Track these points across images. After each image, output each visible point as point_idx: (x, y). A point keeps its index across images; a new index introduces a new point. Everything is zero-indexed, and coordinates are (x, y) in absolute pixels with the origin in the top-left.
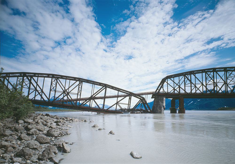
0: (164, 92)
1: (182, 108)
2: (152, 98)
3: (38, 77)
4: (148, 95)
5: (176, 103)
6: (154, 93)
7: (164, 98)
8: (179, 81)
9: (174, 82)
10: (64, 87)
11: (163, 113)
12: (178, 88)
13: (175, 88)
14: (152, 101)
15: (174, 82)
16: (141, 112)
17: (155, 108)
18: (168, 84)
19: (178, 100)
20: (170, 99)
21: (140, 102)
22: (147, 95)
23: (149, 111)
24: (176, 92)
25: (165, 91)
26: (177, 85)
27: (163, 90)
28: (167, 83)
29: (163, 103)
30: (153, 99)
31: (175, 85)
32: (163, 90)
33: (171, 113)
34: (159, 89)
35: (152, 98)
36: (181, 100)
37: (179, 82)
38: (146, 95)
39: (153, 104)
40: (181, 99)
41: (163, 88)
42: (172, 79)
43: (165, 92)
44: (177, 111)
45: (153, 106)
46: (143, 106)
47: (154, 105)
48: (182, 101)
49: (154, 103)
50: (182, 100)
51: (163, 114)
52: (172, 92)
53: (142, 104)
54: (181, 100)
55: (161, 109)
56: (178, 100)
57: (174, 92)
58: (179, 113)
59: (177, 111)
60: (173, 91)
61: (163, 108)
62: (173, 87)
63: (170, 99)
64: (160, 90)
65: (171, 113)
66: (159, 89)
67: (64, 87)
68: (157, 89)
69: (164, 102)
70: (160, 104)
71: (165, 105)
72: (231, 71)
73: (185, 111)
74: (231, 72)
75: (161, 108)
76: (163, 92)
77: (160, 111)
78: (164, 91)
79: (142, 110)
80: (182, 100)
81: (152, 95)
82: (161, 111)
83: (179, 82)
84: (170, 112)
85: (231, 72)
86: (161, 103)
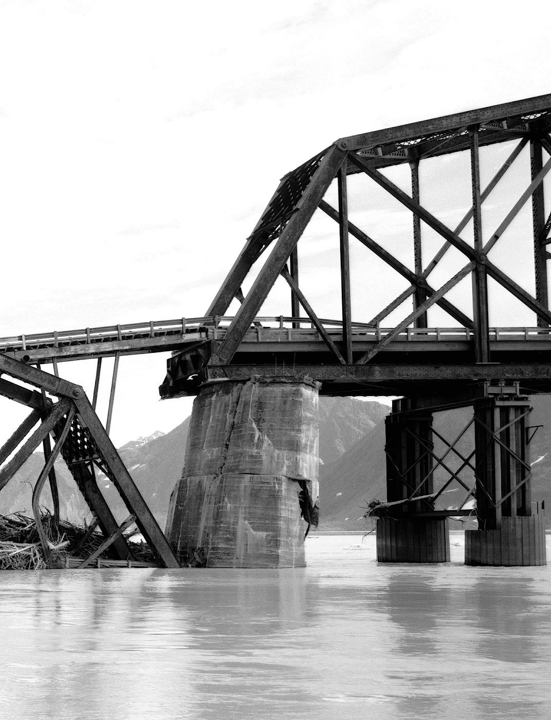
0: (306, 326)
1: (514, 506)
2: (168, 390)
3: (415, 157)
4: (123, 359)
5: (439, 449)
6: (188, 337)
7: (307, 392)
8: (478, 198)
9: (420, 215)
10: (483, 189)
11: (289, 562)
12: (469, 279)
13: (435, 281)
14: (167, 432)
15: (420, 215)
16: (45, 553)
17: (207, 510)
18: (347, 229)
19: (466, 414)
20: (368, 403)
21: (33, 444)
22: (108, 362)
23: (138, 539)
24: (438, 318)
25: (320, 314)
26: (452, 238)
27: (297, 298)
28: (340, 216)
29: (294, 446)
30: (184, 405)
31: (432, 241)
32: (297, 298)
33: (383, 559)
34: (247, 286)
35: (168, 390)
36: (497, 412)
37: (475, 213)
38: (99, 355)
39: (181, 464)
40: (498, 403)
41: (293, 278)
42: (399, 174)
43: (312, 318)
44: (457, 543)
45: (182, 486)
46: (73, 484)
47: (189, 470)
48: (505, 420)
49: (194, 446)
50: (505, 411)
51: (295, 571)
52: (391, 322)
53: (60, 457)
54: (497, 412)
55: (276, 518)
56: (466, 414)
57: (421, 321)
58: (471, 561)
59: (457, 543)
60: (407, 308)
61: (290, 508)
62: (411, 267)
63: (377, 405)
64: (262, 308)
65: (383, 559)
66: (247, 286)
67: (483, 188)
68: (232, 287)
69: (309, 435)
70: (256, 460)
71: (321, 469)
72: (524, 470)
73: (545, 537)
74: (434, 459)
75: (274, 497)
76: (295, 319)
77: (263, 534)
78: (303, 314)
79: (54, 525)
80: (505, 411)
81: (168, 355)
82: (277, 544)
83: (475, 213)
84: (374, 555)
85: (434, 459)
86: (277, 444)
